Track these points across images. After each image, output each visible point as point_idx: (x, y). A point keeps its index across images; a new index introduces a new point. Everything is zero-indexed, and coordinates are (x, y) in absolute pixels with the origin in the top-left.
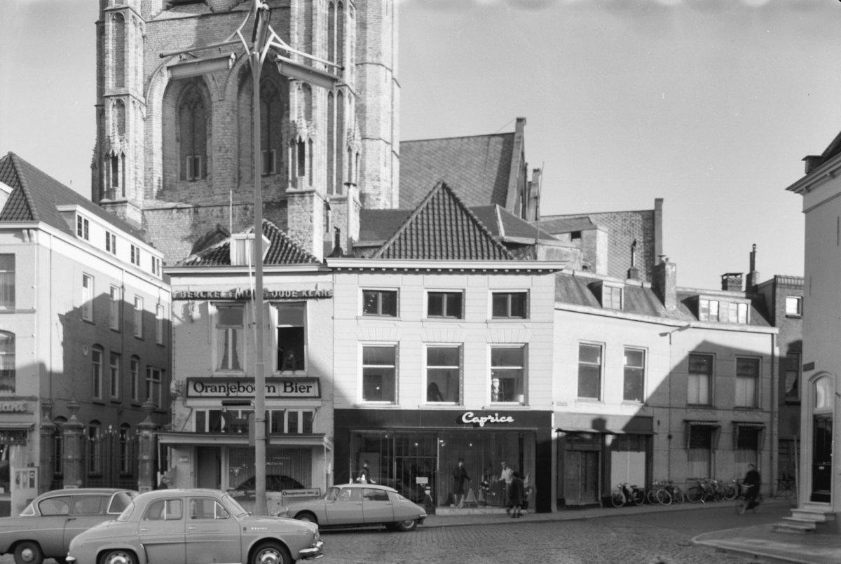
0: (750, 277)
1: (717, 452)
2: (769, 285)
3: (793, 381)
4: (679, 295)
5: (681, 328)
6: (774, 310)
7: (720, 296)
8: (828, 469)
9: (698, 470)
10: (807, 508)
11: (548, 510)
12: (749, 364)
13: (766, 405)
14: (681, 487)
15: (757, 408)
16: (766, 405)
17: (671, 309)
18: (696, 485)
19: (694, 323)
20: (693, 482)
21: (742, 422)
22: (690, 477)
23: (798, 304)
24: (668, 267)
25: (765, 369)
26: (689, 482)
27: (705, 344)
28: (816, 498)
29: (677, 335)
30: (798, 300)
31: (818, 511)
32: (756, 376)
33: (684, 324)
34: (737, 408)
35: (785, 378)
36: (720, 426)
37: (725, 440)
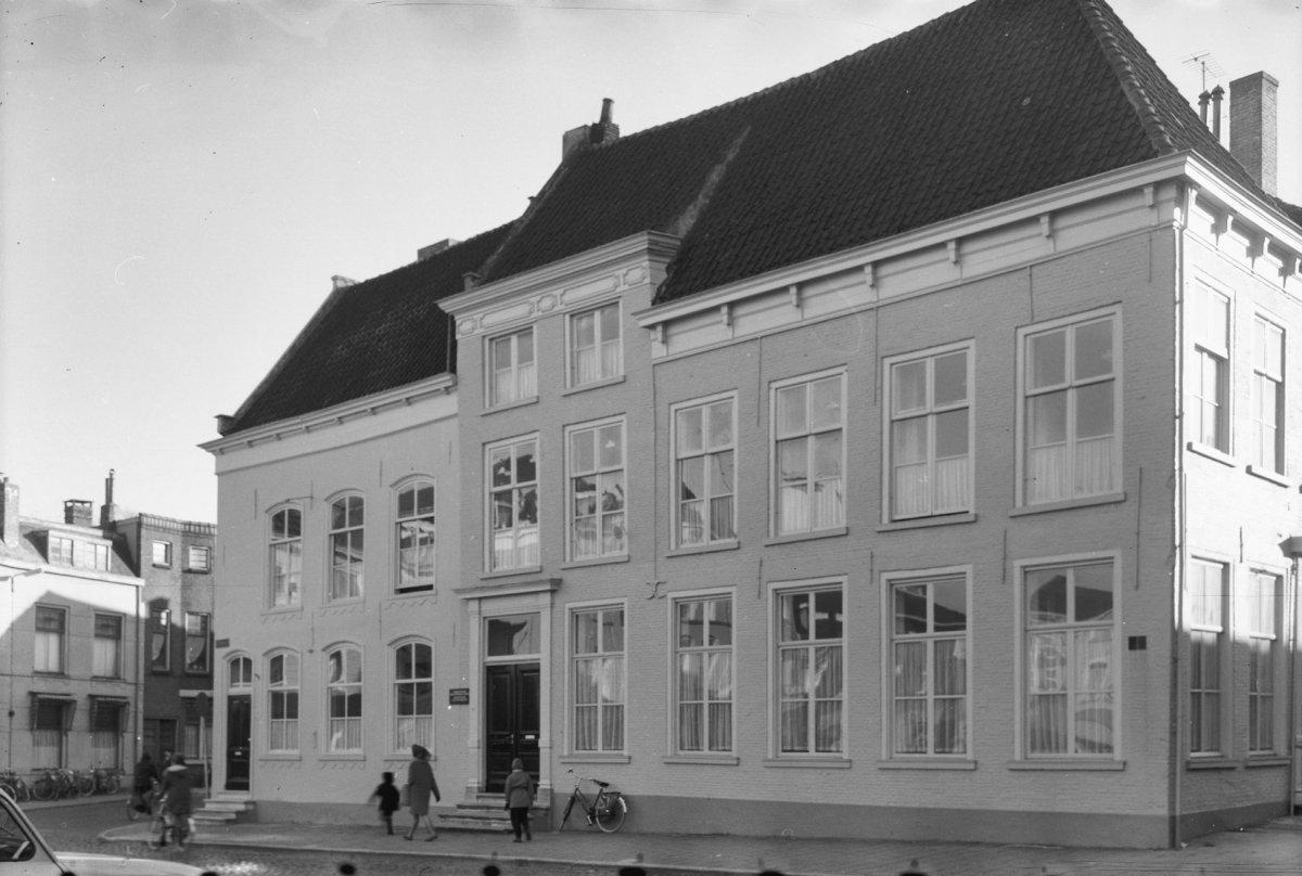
0: (106, 510)
1: (70, 733)
2: (131, 524)
3: (160, 646)
4: (22, 527)
5: (29, 572)
6: (139, 556)
7: (61, 530)
8: (246, 755)
9: (46, 757)
10: (222, 798)
11: (591, 746)
12: (110, 624)
13: (129, 676)
14: (25, 779)
15: (119, 678)
16: (129, 676)
17: (11, 546)
18: (45, 777)
19: (45, 567)
20: (41, 773)
21: (102, 696)
22: (36, 767)
23: (166, 551)
24: (7, 489)
25: (128, 631)
26: (35, 773)
27: (49, 594)
28: (231, 786)
29: (21, 580)
30: (166, 545)
31: (238, 800)
32: (117, 637)
33: (32, 567)
34: (95, 678)
35: (151, 641)
36: (75, 701)
37: (80, 719)
